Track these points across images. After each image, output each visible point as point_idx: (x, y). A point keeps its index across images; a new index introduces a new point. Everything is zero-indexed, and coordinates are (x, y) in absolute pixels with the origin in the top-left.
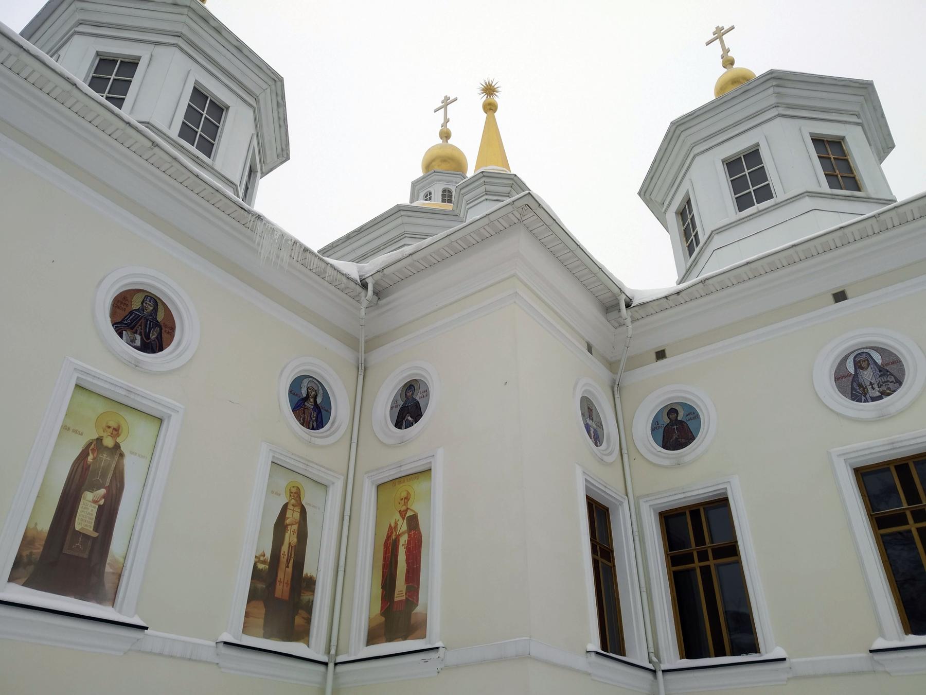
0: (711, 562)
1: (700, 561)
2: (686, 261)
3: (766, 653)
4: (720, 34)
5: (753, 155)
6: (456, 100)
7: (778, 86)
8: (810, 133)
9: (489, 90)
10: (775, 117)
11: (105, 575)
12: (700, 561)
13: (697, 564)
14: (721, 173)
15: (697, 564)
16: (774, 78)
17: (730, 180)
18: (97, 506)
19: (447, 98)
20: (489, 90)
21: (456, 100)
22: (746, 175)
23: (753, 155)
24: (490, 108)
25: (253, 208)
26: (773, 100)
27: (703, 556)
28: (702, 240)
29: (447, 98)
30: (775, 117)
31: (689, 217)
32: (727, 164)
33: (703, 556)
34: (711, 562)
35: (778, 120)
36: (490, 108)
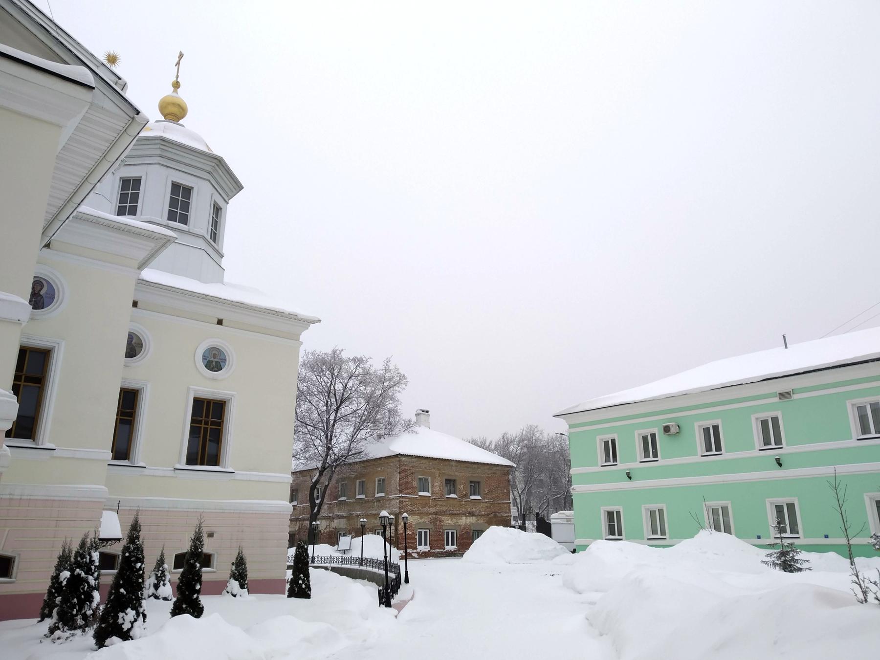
0: (209, 427)
1: (205, 424)
3: (42, 445)
5: (137, 182)
7: (217, 165)
8: (172, 181)
9: (181, 56)
10: (156, 164)
11: (40, 616)
12: (205, 424)
13: (203, 426)
14: (117, 184)
15: (203, 426)
16: (220, 161)
17: (120, 192)
18: (98, 554)
20: (181, 56)
22: (129, 193)
23: (137, 182)
25: (125, 93)
26: (159, 152)
27: (206, 423)
30: (156, 164)
32: (123, 180)
33: (206, 423)
34: (209, 427)
35: (157, 166)
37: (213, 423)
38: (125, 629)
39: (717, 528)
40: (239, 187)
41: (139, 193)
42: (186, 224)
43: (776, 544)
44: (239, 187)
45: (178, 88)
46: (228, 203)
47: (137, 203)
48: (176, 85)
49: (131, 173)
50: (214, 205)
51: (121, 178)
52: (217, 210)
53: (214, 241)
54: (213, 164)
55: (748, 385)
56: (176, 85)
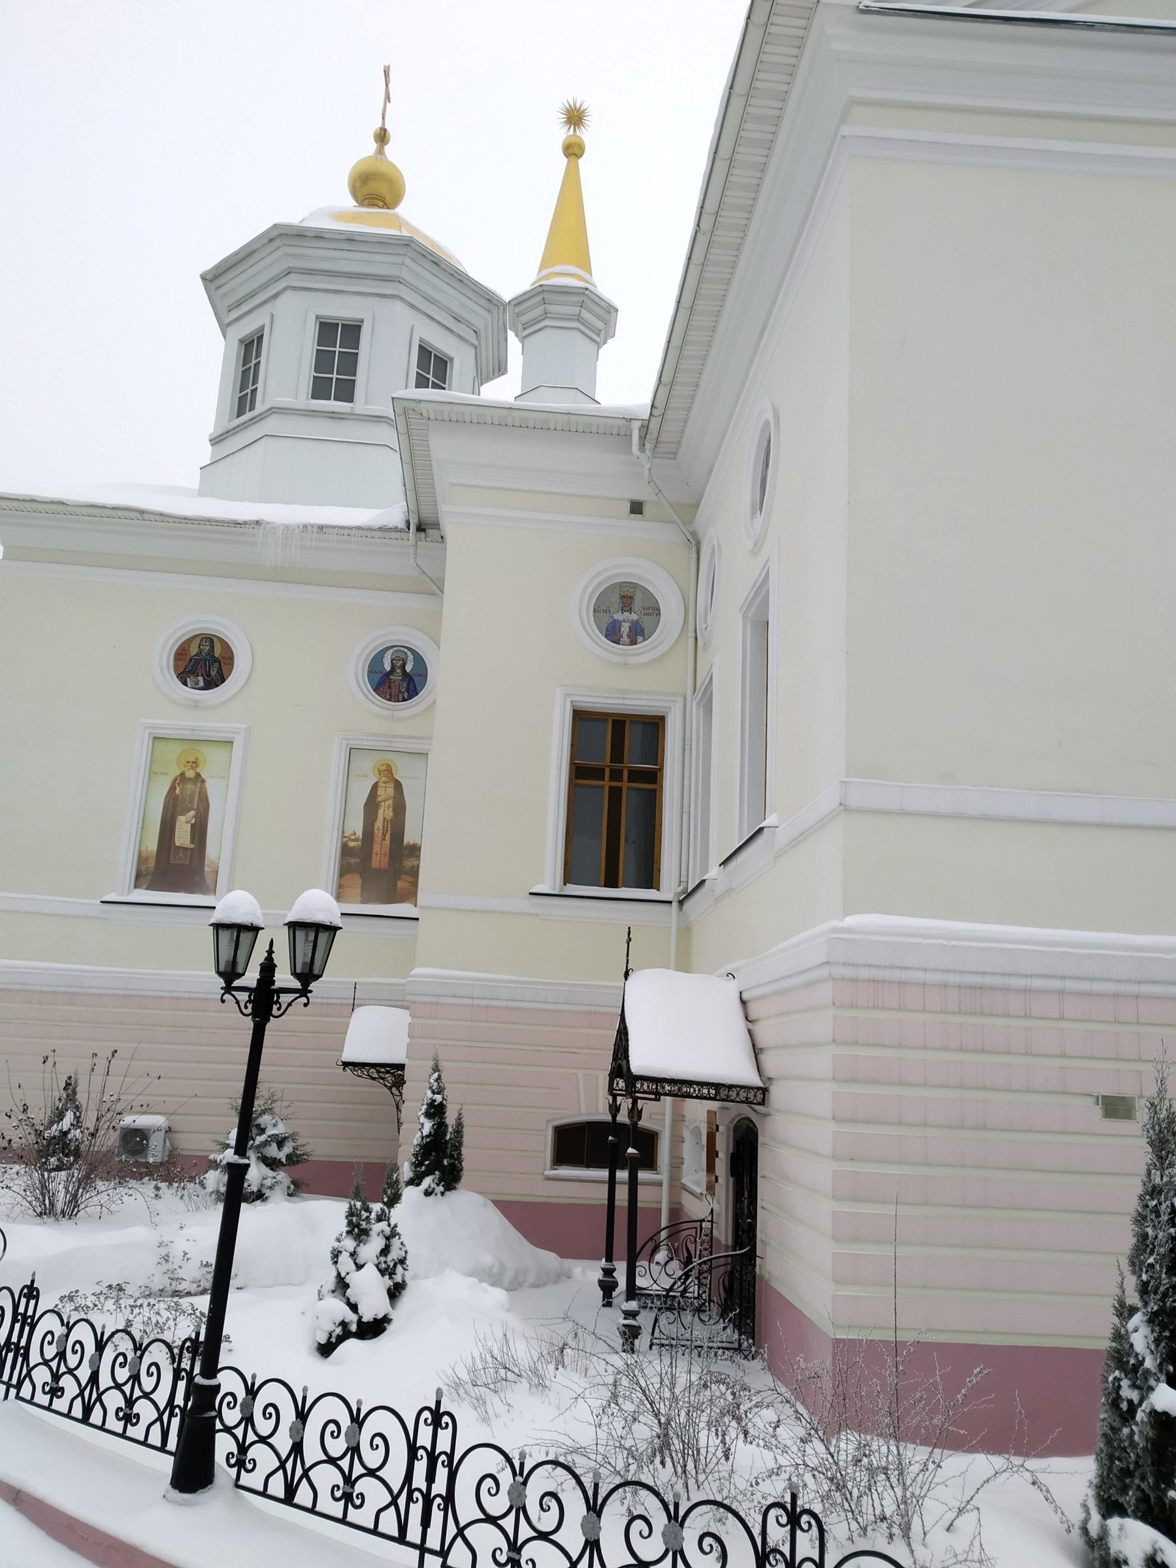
2: (230, 420)
5: (352, 331)
14: (311, 332)
23: (352, 331)
24: (573, 150)
28: (260, 407)
31: (254, 362)
36: (573, 150)
37: (636, 776)
41: (357, 354)
45: (581, 156)
47: (355, 376)
49: (342, 309)
51: (241, 341)
56: (382, 137)
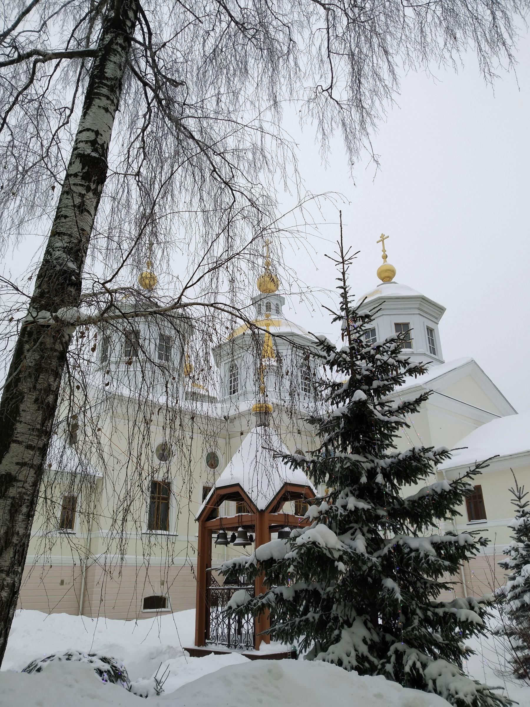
4: (383, 238)
6: (388, 237)
9: (325, 255)
19: (383, 235)
20: (325, 255)
21: (388, 237)
26: (417, 306)
29: (383, 235)
35: (418, 315)
38: (389, 655)
39: (447, 699)
40: (441, 310)
42: (411, 348)
43: (14, 587)
44: (441, 310)
46: (438, 324)
48: (385, 257)
50: (427, 329)
52: (430, 331)
53: (435, 354)
54: (419, 302)
55: (491, 384)
56: (385, 257)
